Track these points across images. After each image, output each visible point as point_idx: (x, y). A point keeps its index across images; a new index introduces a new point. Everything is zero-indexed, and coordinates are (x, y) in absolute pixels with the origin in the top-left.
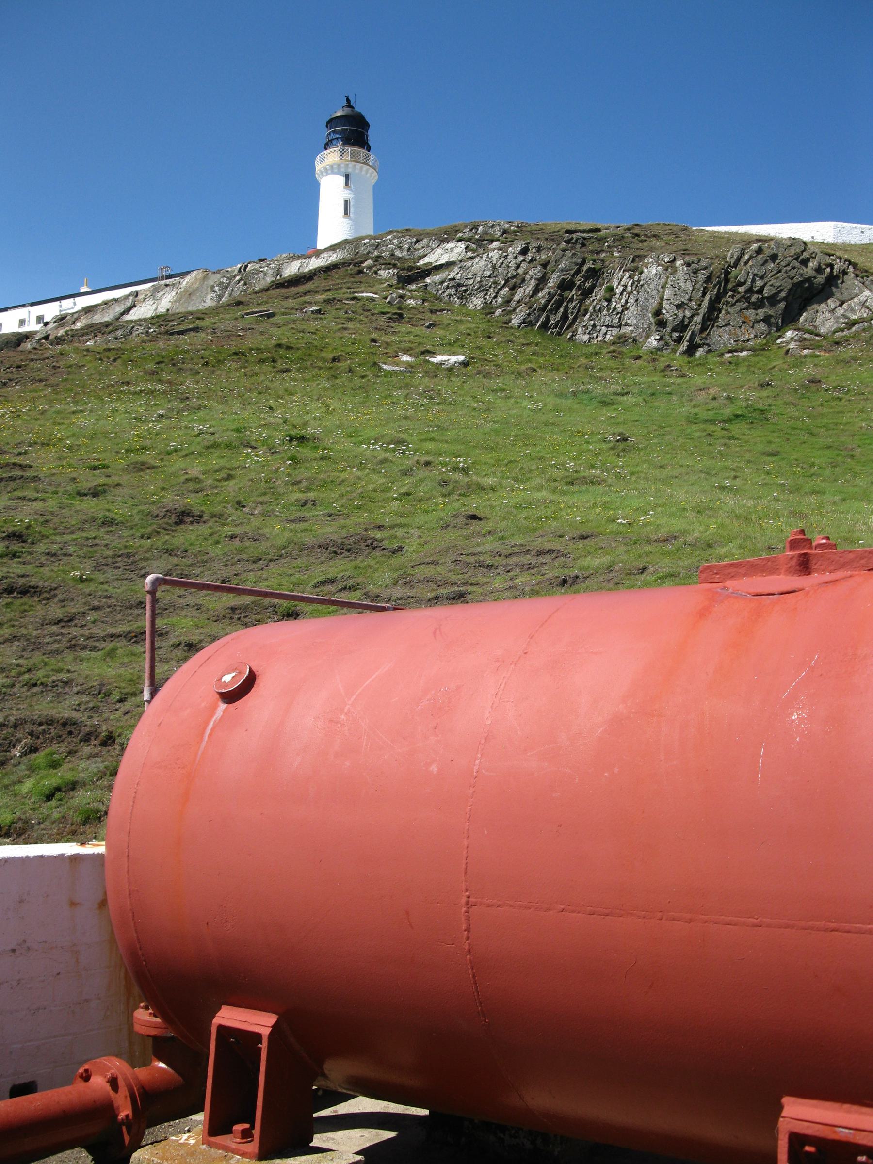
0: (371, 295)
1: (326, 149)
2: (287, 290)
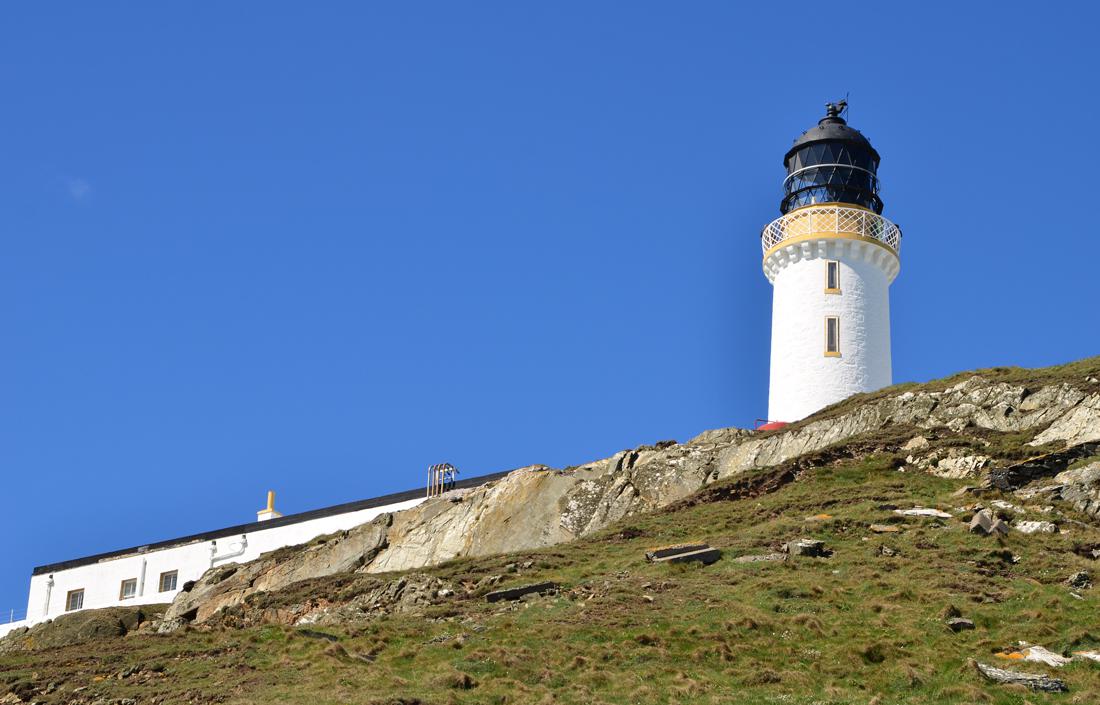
0: (934, 512)
1: (784, 211)
2: (735, 504)
